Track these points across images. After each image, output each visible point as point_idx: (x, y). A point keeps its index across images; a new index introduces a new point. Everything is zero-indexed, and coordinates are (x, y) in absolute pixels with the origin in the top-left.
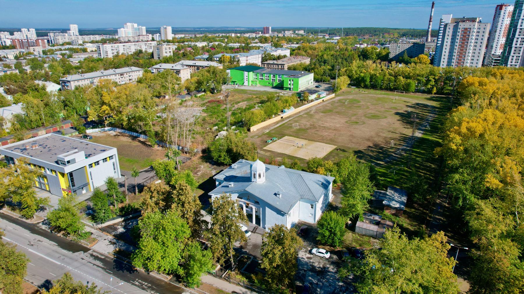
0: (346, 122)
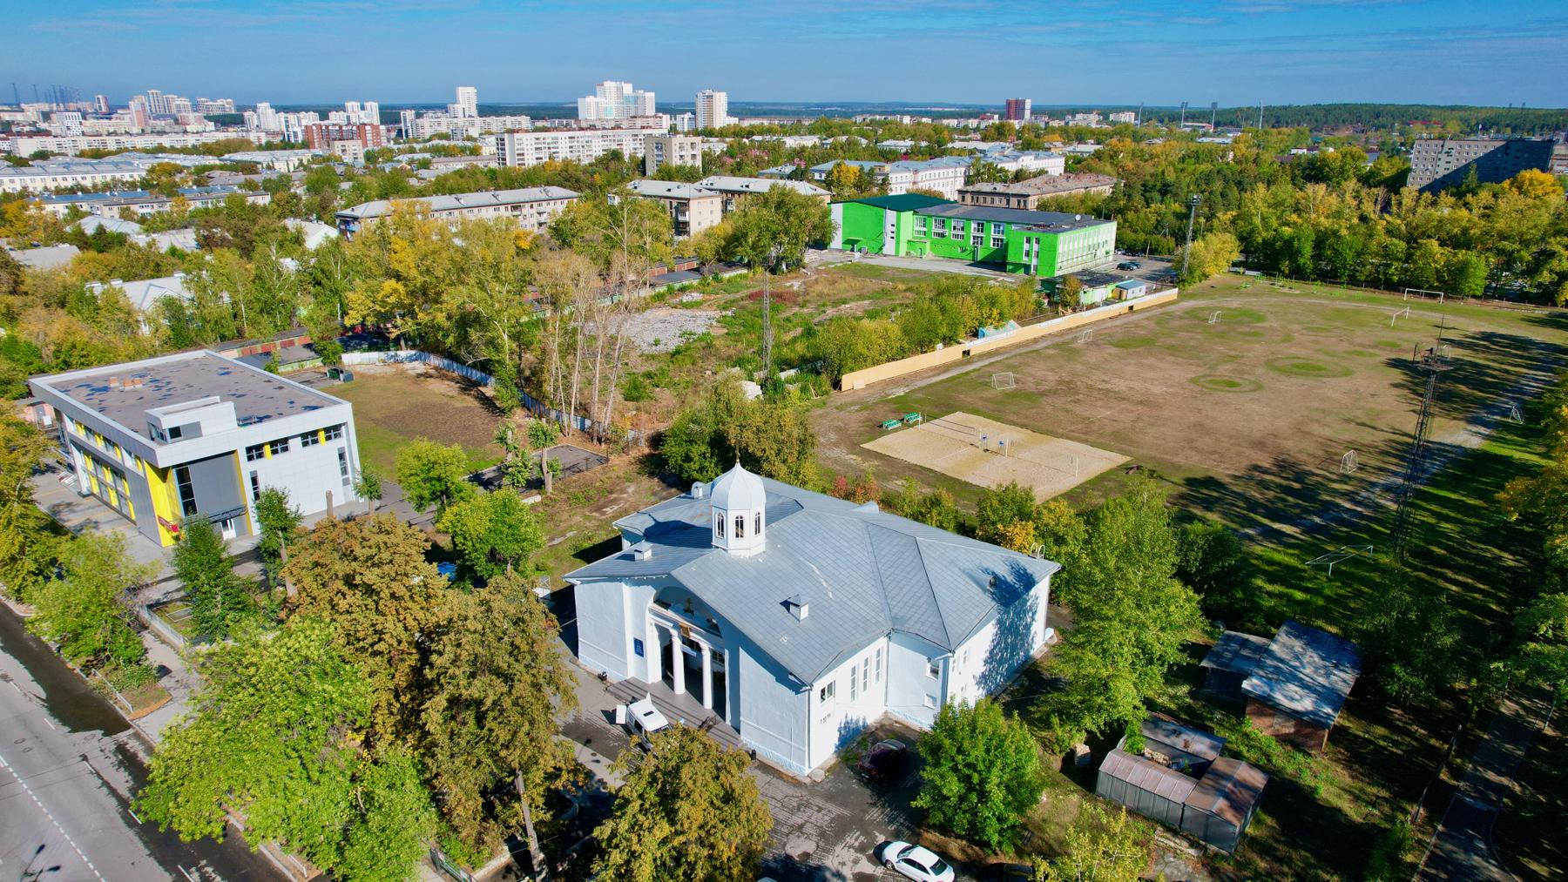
0: (1192, 380)
